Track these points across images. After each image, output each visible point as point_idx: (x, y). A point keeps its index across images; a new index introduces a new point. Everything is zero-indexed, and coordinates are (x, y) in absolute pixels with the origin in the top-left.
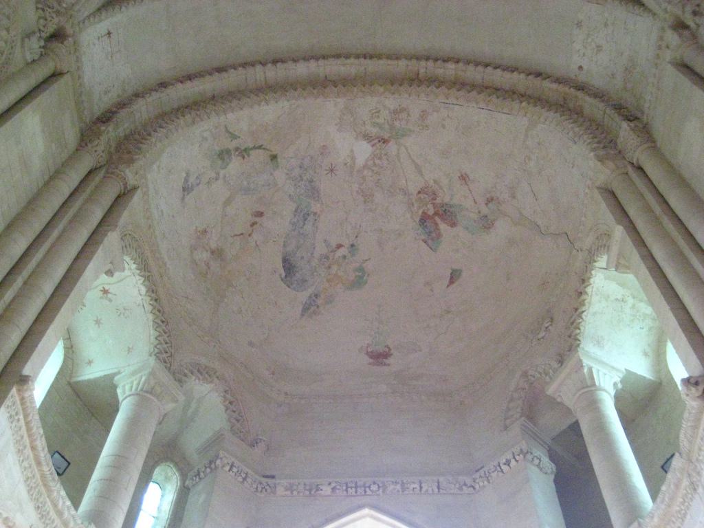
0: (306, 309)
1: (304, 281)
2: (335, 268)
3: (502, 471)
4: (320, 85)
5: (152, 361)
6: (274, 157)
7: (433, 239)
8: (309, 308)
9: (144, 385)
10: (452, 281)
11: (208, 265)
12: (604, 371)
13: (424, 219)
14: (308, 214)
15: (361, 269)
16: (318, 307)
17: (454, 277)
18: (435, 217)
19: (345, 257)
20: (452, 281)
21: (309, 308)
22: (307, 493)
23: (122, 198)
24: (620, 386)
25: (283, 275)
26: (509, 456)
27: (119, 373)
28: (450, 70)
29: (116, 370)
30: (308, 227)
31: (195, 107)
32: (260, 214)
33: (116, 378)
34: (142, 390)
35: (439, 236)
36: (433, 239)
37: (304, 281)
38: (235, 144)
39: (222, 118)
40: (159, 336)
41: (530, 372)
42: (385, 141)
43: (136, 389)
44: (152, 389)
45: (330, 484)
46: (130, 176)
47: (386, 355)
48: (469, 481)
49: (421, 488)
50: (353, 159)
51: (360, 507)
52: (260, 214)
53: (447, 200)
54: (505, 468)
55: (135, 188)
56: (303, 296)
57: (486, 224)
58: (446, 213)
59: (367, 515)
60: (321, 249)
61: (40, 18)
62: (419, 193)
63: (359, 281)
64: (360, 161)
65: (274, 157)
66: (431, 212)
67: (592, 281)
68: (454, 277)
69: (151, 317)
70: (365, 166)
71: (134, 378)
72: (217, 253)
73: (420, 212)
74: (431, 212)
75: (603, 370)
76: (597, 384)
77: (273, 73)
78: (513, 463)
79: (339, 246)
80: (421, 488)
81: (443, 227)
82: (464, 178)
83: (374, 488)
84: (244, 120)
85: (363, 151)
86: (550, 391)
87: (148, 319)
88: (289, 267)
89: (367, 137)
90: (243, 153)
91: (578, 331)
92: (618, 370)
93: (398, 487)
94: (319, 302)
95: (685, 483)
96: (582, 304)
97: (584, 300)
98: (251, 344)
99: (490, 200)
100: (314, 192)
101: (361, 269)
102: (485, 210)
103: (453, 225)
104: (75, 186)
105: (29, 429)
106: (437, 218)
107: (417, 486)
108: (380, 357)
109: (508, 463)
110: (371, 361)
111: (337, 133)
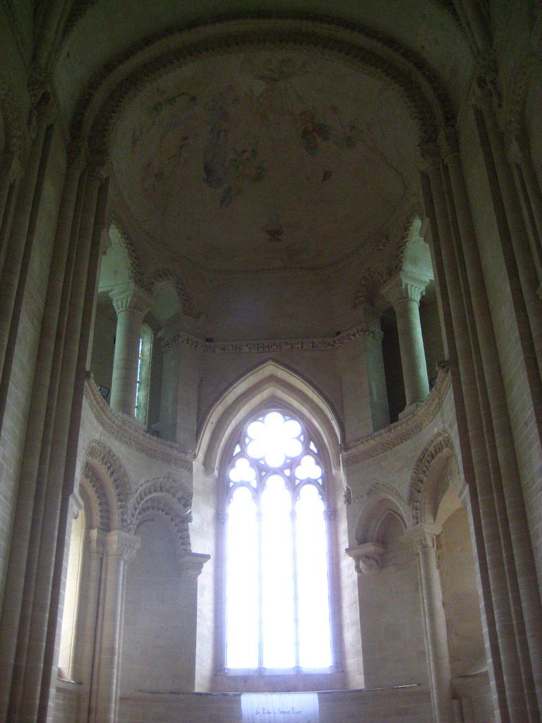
0: (222, 202)
3: (351, 339)
4: (225, 44)
5: (132, 286)
6: (193, 99)
9: (130, 304)
10: (324, 179)
12: (415, 285)
13: (305, 133)
14: (220, 132)
16: (231, 197)
17: (326, 176)
18: (313, 133)
19: (248, 159)
20: (324, 179)
22: (234, 351)
23: (103, 190)
24: (424, 293)
25: (206, 177)
26: (355, 331)
27: (112, 290)
29: (110, 288)
31: (133, 82)
33: (110, 294)
34: (129, 307)
40: (134, 263)
41: (372, 269)
42: (276, 80)
43: (126, 307)
44: (136, 304)
45: (247, 345)
46: (103, 173)
47: (279, 232)
48: (331, 343)
49: (302, 347)
51: (266, 361)
52: (186, 138)
54: (353, 338)
55: (107, 179)
58: (322, 131)
59: (270, 364)
61: (31, 96)
62: (302, 115)
65: (193, 99)
66: (310, 129)
67: (413, 224)
68: (326, 176)
69: (126, 250)
71: (122, 296)
73: (303, 128)
74: (310, 129)
75: (412, 283)
76: (410, 296)
77: (188, 37)
78: (357, 335)
79: (244, 152)
80: (302, 347)
82: (334, 109)
83: (274, 347)
85: (260, 87)
86: (382, 292)
87: (124, 252)
88: (209, 170)
90: (171, 101)
91: (402, 255)
92: (425, 282)
93: (289, 347)
95: (436, 401)
96: (407, 236)
97: (408, 234)
99: (353, 128)
103: (326, 139)
104: (211, 630)
105: (96, 399)
106: (314, 133)
107: (300, 346)
110: (269, 237)
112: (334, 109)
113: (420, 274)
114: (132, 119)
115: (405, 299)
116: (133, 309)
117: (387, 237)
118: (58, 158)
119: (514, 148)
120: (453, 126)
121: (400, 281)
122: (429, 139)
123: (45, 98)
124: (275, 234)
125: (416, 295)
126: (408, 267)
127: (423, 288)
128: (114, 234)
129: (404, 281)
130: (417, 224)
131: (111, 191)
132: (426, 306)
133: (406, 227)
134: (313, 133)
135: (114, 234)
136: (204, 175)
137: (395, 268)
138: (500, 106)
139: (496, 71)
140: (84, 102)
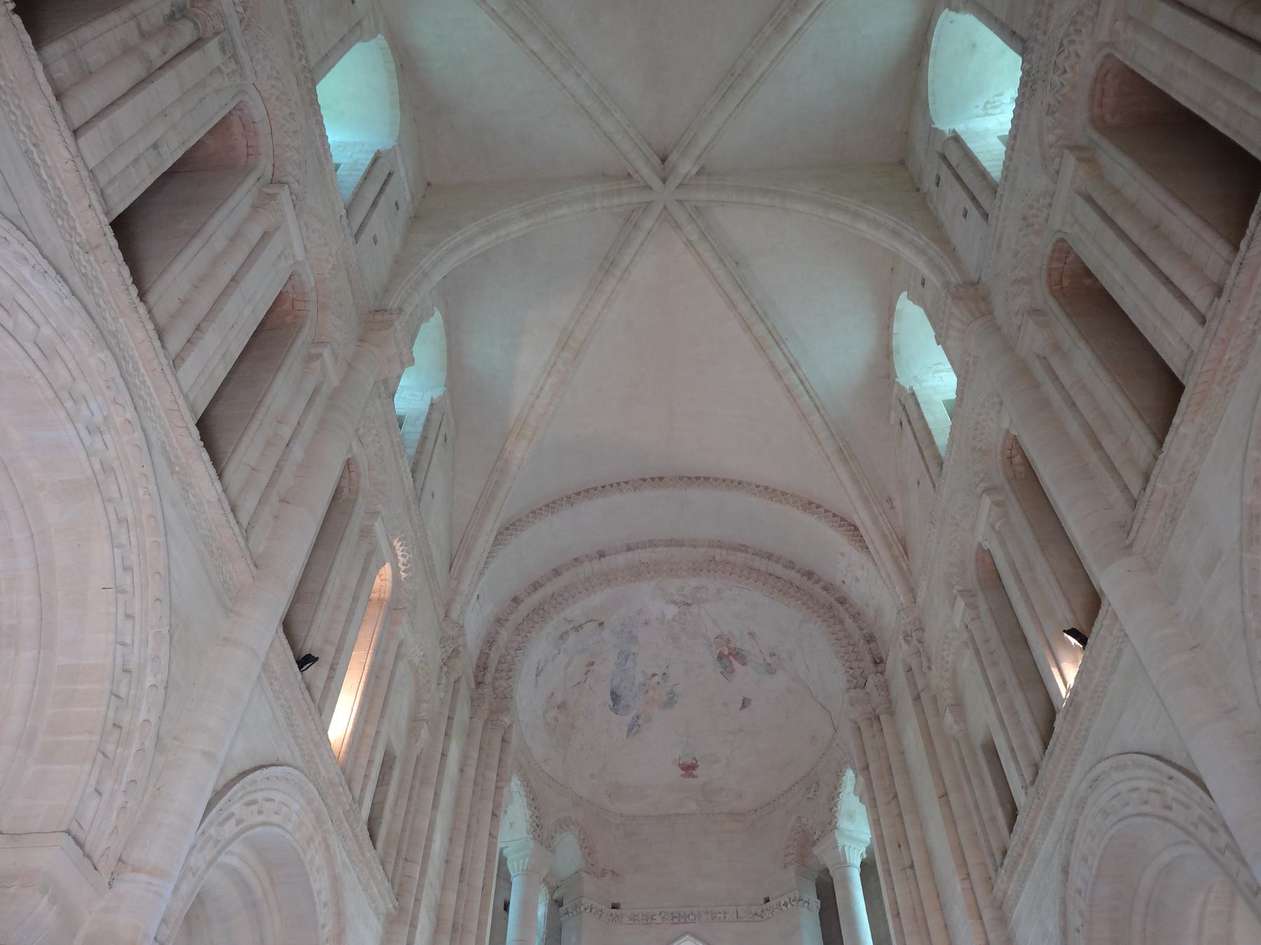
0: (630, 730)
1: (628, 706)
2: (651, 692)
6: (602, 624)
7: (728, 671)
8: (633, 729)
11: (556, 719)
13: (721, 657)
15: (672, 692)
17: (745, 703)
18: (729, 657)
20: (744, 706)
21: (633, 729)
28: (740, 558)
30: (630, 664)
32: (592, 664)
35: (733, 671)
36: (728, 671)
37: (628, 706)
38: (571, 626)
39: (562, 615)
48: (759, 912)
50: (664, 616)
51: (683, 935)
52: (592, 664)
53: (739, 645)
55: (510, 726)
56: (628, 719)
57: (770, 670)
58: (738, 654)
60: (639, 679)
63: (670, 702)
64: (669, 616)
65: (602, 624)
66: (726, 652)
68: (745, 703)
70: (674, 619)
72: (562, 706)
74: (726, 652)
79: (654, 675)
81: (736, 664)
82: (752, 634)
84: (575, 611)
85: (671, 611)
88: (615, 697)
89: (675, 603)
90: (577, 629)
94: (640, 722)
98: (592, 776)
99: (772, 655)
100: (633, 639)
101: (672, 692)
102: (769, 660)
103: (744, 664)
108: (689, 769)
109: (786, 904)
111: (651, 601)
112: (752, 634)
113: (855, 834)
114: (540, 647)
115: (844, 865)
116: (528, 873)
117: (817, 783)
118: (463, 713)
119: (949, 718)
120: (882, 673)
121: (835, 841)
122: (859, 683)
123: (456, 652)
124: (689, 769)
125: (855, 858)
126: (843, 823)
127: (863, 850)
128: (515, 784)
129: (841, 842)
130: (850, 775)
131: (514, 740)
132: (867, 868)
133: (839, 775)
134: (729, 657)
135: (515, 784)
136: (611, 703)
137: (830, 825)
138: (929, 668)
139: (922, 630)
140: (490, 642)
